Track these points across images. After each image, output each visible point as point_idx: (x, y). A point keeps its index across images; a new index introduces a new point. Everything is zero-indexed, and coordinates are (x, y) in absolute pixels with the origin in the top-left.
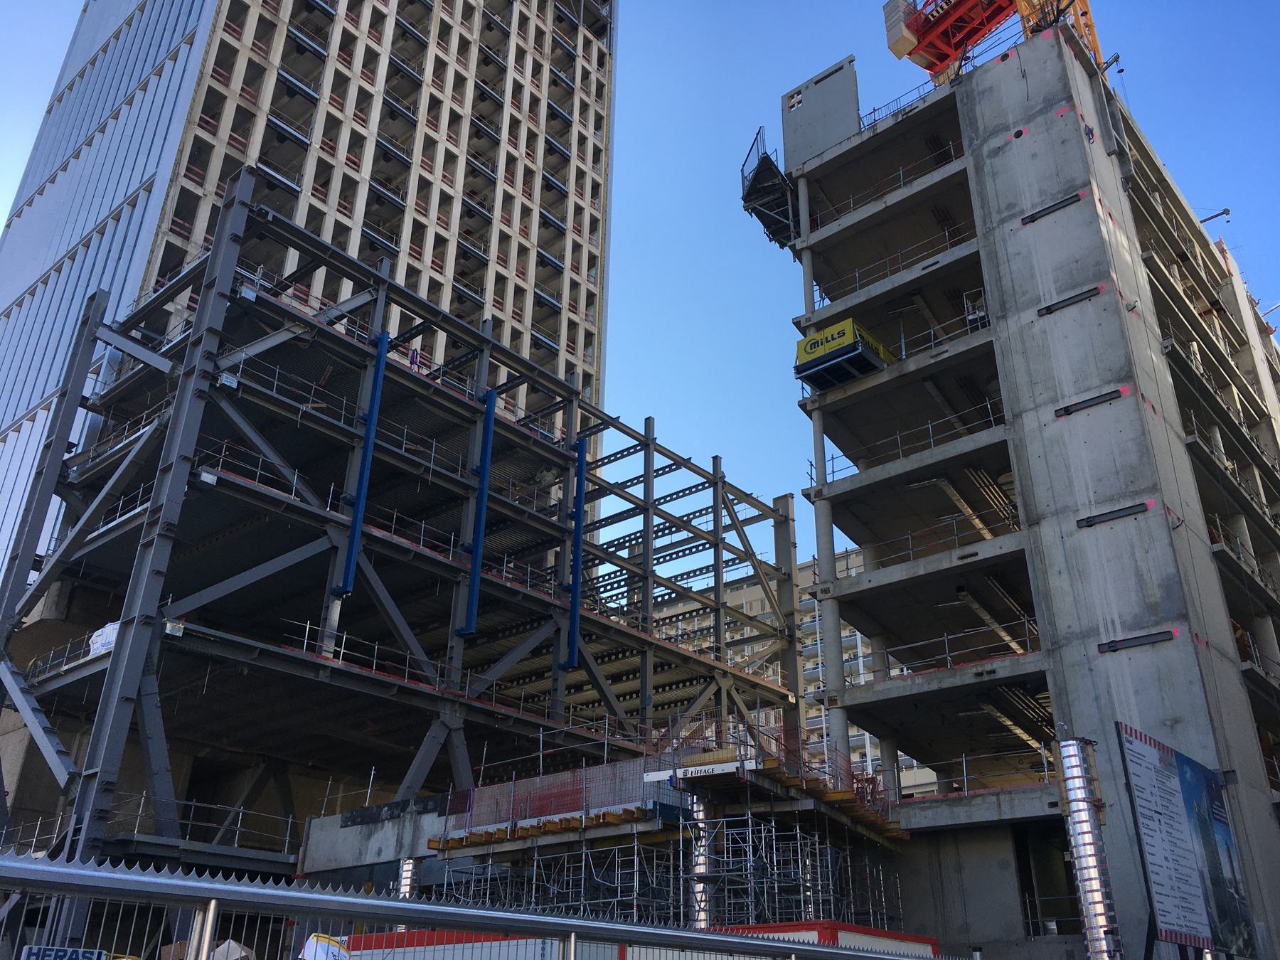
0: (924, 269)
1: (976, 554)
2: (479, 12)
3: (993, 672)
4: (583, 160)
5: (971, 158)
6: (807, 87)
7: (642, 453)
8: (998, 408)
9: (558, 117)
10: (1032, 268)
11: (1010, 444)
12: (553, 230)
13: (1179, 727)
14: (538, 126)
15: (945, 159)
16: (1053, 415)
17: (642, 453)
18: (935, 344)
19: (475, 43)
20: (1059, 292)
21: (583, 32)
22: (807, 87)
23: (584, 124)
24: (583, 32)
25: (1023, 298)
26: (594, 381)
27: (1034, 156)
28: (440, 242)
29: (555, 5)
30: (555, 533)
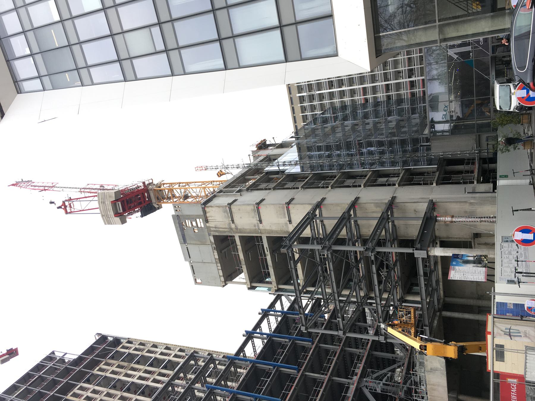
0: (267, 251)
2: (110, 391)
4: (131, 348)
5: (236, 234)
6: (195, 277)
7: (254, 339)
9: (113, 356)
10: (276, 224)
11: (268, 235)
12: (143, 360)
13: (416, 210)
15: (234, 242)
16: (291, 225)
17: (254, 339)
19: (122, 394)
20: (285, 218)
21: (119, 349)
22: (195, 277)
23: (156, 353)
24: (119, 349)
25: (285, 227)
26: (183, 348)
27: (241, 218)
30: (253, 368)
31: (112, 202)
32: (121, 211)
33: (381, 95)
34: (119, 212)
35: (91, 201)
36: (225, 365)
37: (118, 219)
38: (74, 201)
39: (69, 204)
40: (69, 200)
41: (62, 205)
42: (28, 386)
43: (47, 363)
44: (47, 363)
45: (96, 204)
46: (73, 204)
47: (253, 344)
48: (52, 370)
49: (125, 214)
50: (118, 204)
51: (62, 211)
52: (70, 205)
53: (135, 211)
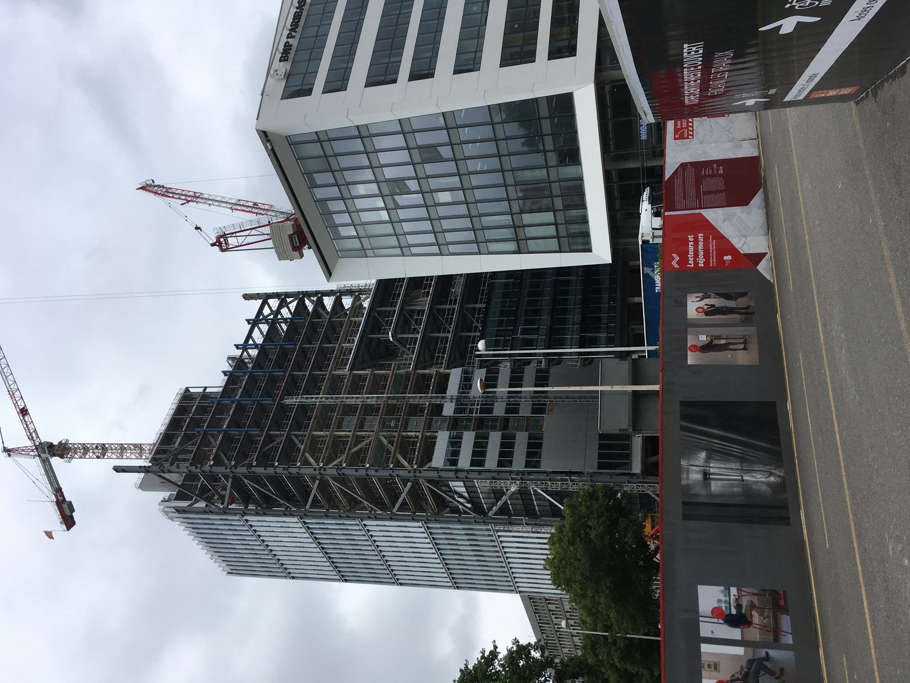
32: (298, 245)
34: (296, 245)
35: (247, 236)
37: (297, 253)
38: (228, 237)
41: (216, 242)
42: (185, 431)
43: (190, 403)
44: (190, 403)
47: (259, 329)
48: (203, 410)
50: (295, 237)
52: (225, 240)
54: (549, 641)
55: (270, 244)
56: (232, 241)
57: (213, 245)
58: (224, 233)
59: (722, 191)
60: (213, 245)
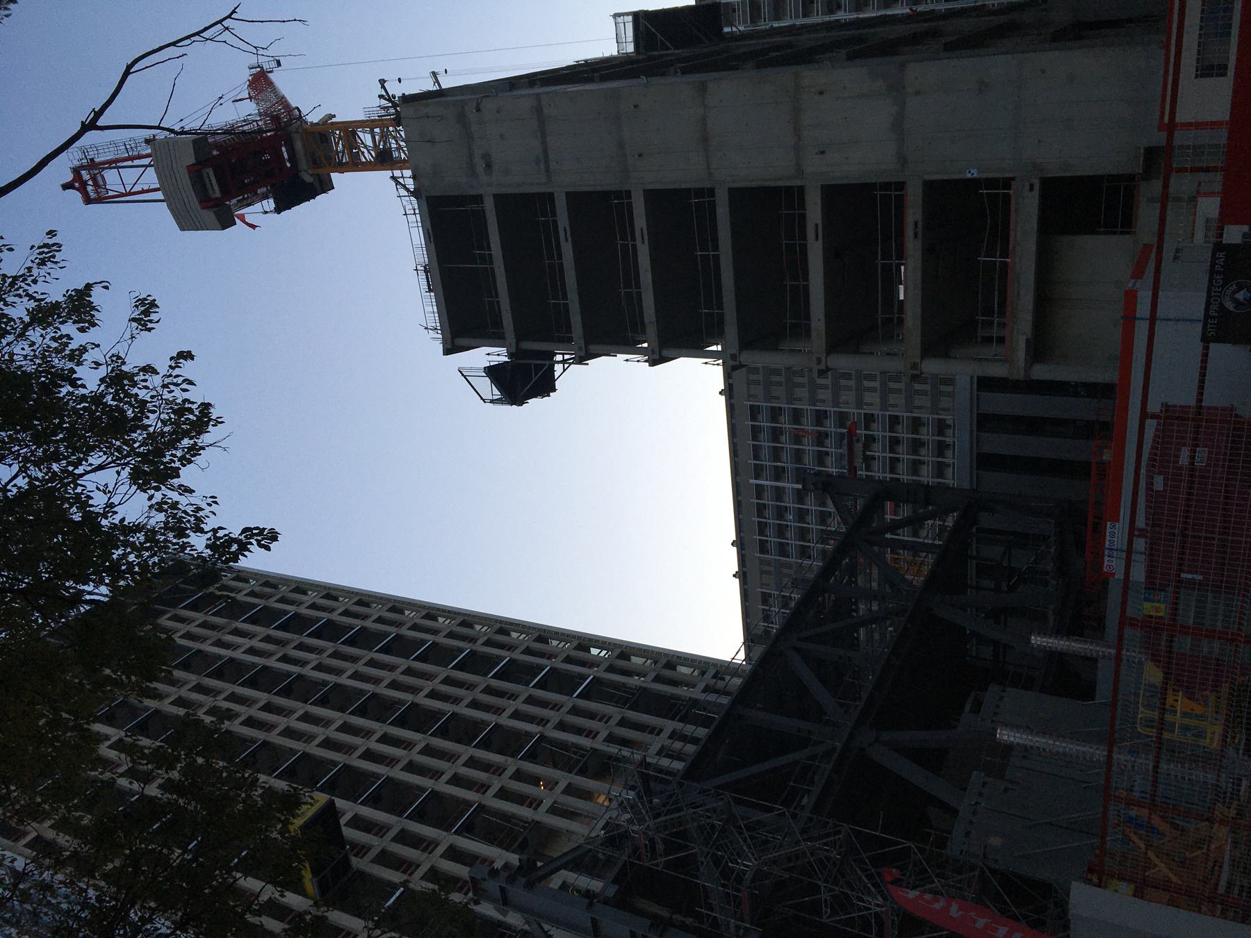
0: (567, 240)
1: (817, 225)
3: (916, 223)
8: (700, 192)
14: (292, 640)
18: (632, 241)
28: (385, 739)
29: (181, 608)
31: (188, 167)
32: (218, 194)
33: (1224, 158)
36: (706, 722)
37: (209, 215)
39: (91, 178)
40: (88, 165)
41: (74, 180)
45: (151, 178)
46: (103, 178)
49: (228, 203)
50: (208, 174)
51: (75, 195)
52: (94, 178)
53: (256, 193)
54: (1166, 119)
55: (159, 195)
56: (111, 178)
57: (66, 187)
58: (92, 160)
59: (1139, 319)
60: (66, 187)
